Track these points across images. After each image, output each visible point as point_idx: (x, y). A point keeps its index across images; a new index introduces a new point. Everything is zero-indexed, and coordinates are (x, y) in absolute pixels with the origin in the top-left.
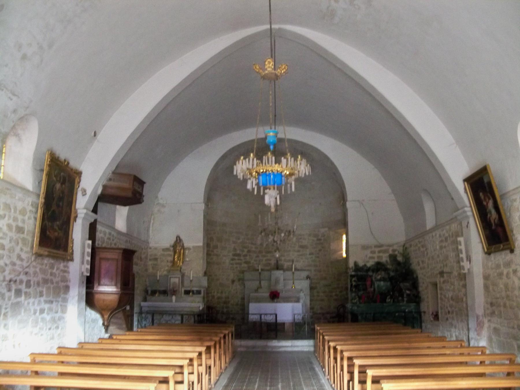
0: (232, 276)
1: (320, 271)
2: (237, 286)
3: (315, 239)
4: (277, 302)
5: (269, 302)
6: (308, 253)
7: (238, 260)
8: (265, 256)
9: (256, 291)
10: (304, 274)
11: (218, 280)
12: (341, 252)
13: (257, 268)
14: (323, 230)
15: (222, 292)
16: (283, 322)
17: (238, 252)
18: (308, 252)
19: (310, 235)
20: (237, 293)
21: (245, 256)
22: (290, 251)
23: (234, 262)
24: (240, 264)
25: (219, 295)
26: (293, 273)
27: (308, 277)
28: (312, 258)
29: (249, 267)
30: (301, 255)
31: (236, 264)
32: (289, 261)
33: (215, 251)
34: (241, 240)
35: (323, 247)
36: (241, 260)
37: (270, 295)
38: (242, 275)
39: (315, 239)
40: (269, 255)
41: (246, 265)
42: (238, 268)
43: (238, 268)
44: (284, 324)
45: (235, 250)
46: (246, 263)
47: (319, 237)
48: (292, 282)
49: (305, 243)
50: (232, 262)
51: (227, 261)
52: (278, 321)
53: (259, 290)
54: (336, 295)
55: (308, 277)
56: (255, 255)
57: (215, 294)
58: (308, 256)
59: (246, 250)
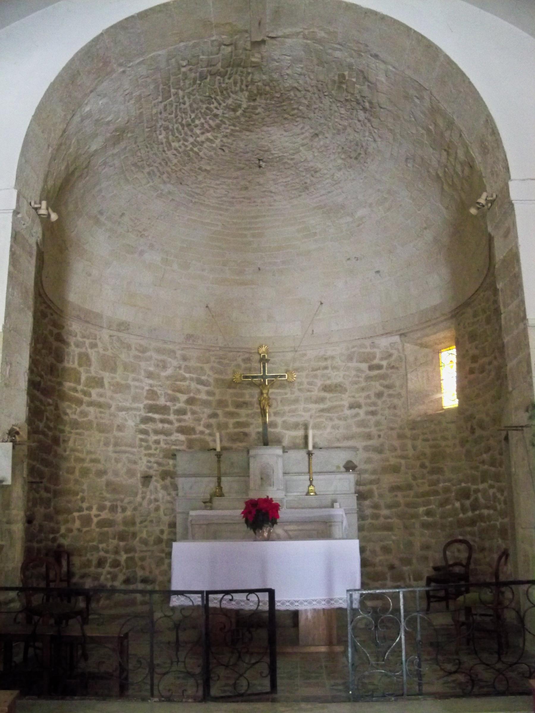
0: (142, 467)
1: (379, 450)
2: (157, 491)
3: (364, 366)
4: (268, 539)
5: (244, 538)
6: (346, 404)
7: (162, 421)
8: (232, 415)
9: (208, 503)
10: (340, 458)
11: (101, 473)
12: (438, 396)
13: (212, 445)
14: (384, 342)
15: (113, 509)
16: (292, 608)
17: (162, 401)
18: (345, 400)
19: (350, 358)
20: (157, 509)
21: (181, 412)
22: (296, 401)
23: (150, 426)
24: (167, 433)
25: (105, 515)
26: (310, 454)
27: (350, 467)
28: (357, 415)
29: (190, 444)
30: (328, 410)
31: (156, 432)
32: (296, 426)
33: (94, 392)
34: (169, 372)
35: (388, 387)
36: (170, 422)
37: (246, 513)
38: (171, 462)
39: (364, 366)
40: (243, 411)
41: (182, 437)
42: (162, 445)
43: (162, 445)
44: (295, 614)
45: (152, 394)
46: (182, 430)
47: (376, 362)
48: (307, 477)
49: (336, 377)
50: (143, 426)
51: (131, 423)
52: (279, 606)
53: (217, 501)
54: (428, 513)
55: (350, 467)
56: (208, 411)
57: (94, 512)
58: (348, 412)
59: (183, 397)
